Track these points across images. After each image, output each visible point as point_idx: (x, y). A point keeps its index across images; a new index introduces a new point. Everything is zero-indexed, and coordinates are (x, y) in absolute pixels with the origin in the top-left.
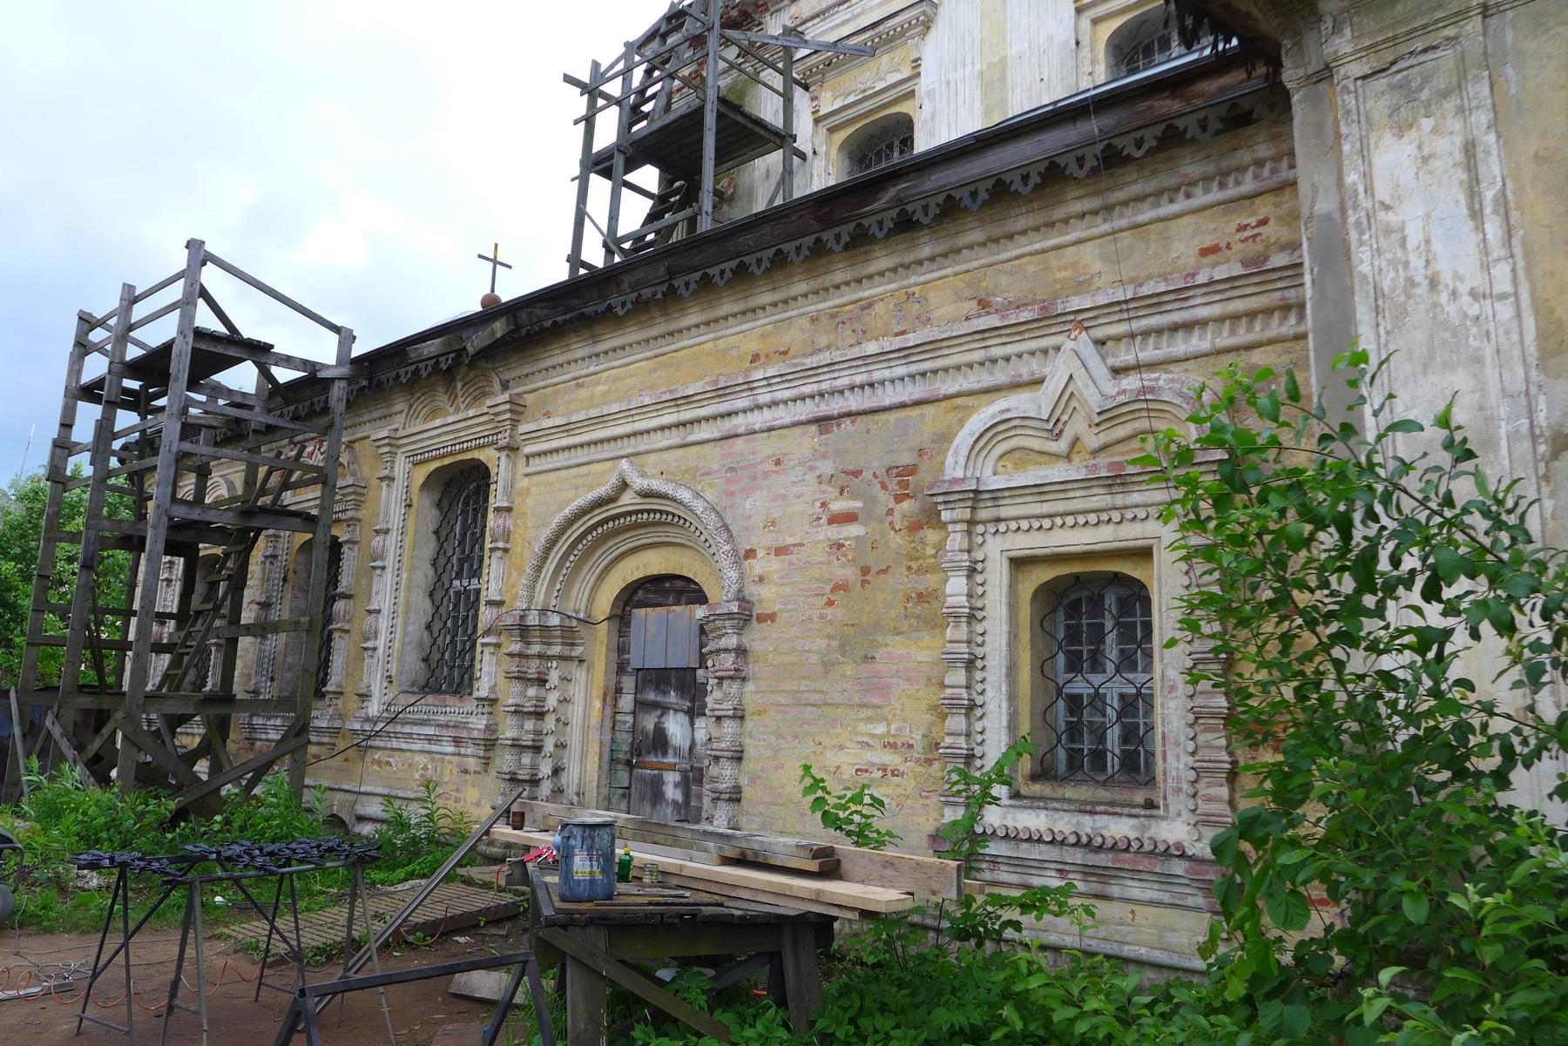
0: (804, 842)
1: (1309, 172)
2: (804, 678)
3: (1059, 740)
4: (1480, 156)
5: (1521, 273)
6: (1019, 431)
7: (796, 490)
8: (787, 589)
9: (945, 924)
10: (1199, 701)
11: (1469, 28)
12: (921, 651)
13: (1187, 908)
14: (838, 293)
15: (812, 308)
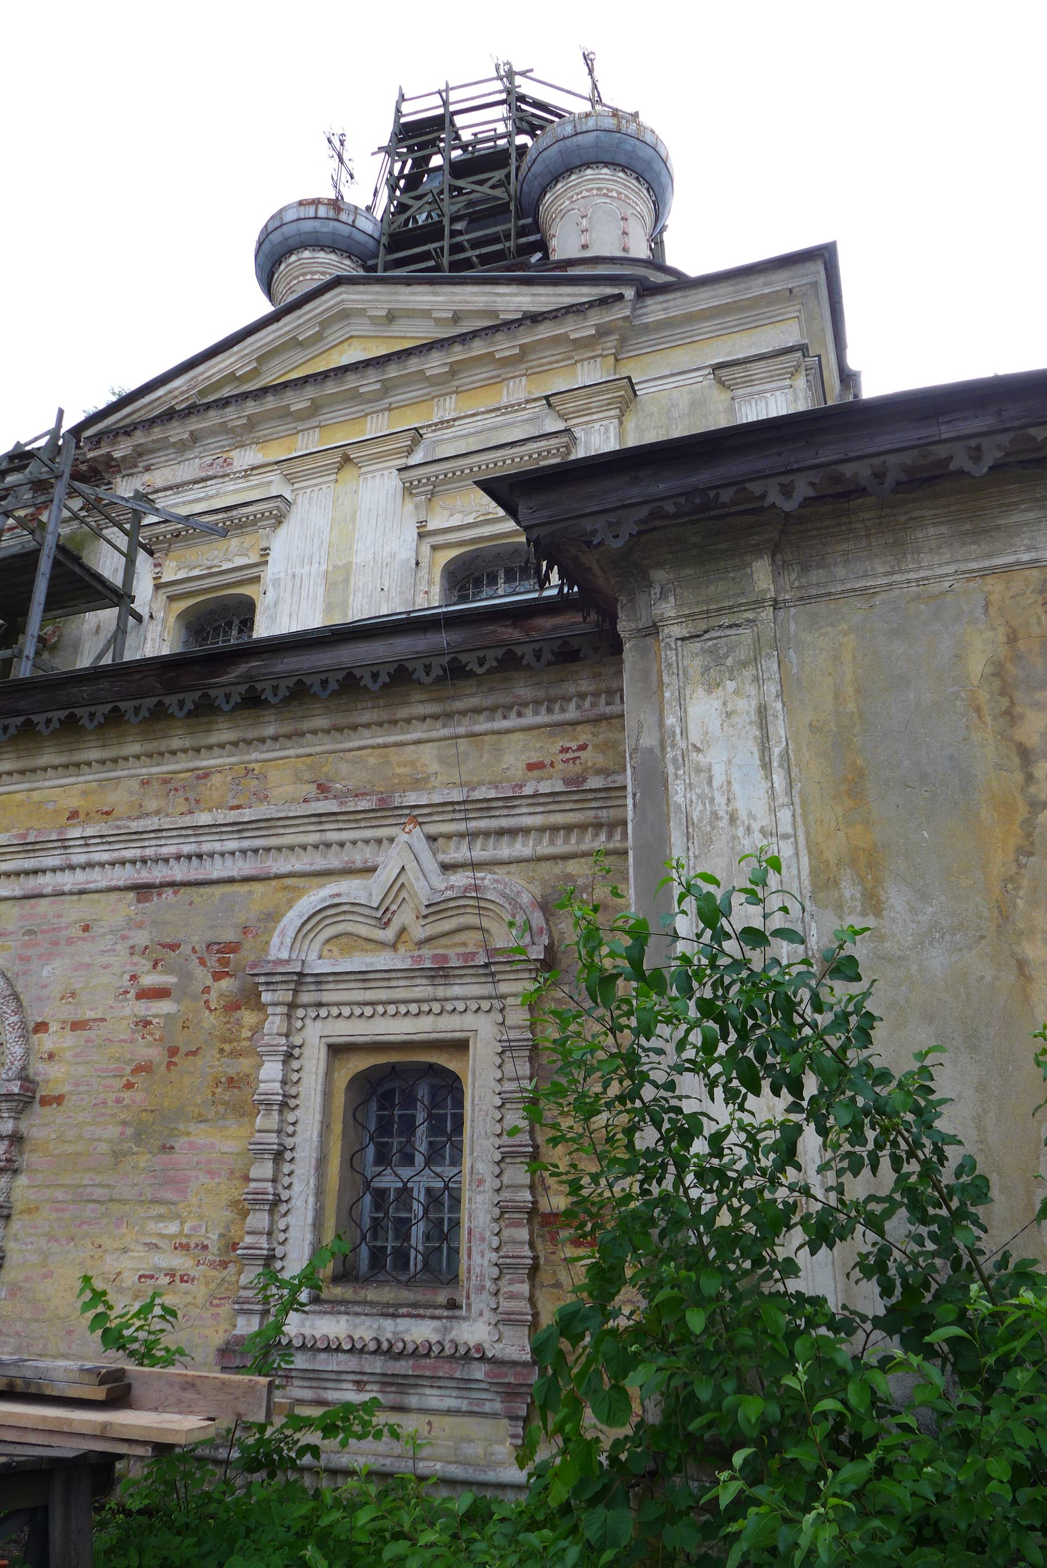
0: (89, 1365)
1: (633, 707)
2: (89, 1170)
3: (364, 1238)
4: (770, 718)
5: (798, 818)
6: (351, 917)
7: (104, 959)
8: (81, 1069)
9: (235, 1454)
10: (505, 1195)
11: (764, 615)
12: (226, 1141)
13: (484, 1415)
14: (173, 758)
15: (144, 771)
